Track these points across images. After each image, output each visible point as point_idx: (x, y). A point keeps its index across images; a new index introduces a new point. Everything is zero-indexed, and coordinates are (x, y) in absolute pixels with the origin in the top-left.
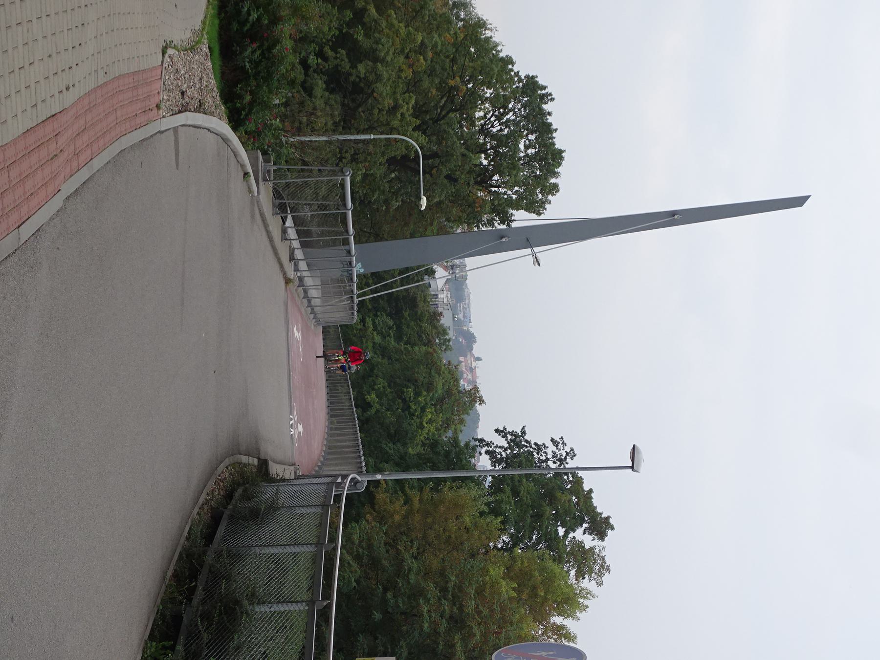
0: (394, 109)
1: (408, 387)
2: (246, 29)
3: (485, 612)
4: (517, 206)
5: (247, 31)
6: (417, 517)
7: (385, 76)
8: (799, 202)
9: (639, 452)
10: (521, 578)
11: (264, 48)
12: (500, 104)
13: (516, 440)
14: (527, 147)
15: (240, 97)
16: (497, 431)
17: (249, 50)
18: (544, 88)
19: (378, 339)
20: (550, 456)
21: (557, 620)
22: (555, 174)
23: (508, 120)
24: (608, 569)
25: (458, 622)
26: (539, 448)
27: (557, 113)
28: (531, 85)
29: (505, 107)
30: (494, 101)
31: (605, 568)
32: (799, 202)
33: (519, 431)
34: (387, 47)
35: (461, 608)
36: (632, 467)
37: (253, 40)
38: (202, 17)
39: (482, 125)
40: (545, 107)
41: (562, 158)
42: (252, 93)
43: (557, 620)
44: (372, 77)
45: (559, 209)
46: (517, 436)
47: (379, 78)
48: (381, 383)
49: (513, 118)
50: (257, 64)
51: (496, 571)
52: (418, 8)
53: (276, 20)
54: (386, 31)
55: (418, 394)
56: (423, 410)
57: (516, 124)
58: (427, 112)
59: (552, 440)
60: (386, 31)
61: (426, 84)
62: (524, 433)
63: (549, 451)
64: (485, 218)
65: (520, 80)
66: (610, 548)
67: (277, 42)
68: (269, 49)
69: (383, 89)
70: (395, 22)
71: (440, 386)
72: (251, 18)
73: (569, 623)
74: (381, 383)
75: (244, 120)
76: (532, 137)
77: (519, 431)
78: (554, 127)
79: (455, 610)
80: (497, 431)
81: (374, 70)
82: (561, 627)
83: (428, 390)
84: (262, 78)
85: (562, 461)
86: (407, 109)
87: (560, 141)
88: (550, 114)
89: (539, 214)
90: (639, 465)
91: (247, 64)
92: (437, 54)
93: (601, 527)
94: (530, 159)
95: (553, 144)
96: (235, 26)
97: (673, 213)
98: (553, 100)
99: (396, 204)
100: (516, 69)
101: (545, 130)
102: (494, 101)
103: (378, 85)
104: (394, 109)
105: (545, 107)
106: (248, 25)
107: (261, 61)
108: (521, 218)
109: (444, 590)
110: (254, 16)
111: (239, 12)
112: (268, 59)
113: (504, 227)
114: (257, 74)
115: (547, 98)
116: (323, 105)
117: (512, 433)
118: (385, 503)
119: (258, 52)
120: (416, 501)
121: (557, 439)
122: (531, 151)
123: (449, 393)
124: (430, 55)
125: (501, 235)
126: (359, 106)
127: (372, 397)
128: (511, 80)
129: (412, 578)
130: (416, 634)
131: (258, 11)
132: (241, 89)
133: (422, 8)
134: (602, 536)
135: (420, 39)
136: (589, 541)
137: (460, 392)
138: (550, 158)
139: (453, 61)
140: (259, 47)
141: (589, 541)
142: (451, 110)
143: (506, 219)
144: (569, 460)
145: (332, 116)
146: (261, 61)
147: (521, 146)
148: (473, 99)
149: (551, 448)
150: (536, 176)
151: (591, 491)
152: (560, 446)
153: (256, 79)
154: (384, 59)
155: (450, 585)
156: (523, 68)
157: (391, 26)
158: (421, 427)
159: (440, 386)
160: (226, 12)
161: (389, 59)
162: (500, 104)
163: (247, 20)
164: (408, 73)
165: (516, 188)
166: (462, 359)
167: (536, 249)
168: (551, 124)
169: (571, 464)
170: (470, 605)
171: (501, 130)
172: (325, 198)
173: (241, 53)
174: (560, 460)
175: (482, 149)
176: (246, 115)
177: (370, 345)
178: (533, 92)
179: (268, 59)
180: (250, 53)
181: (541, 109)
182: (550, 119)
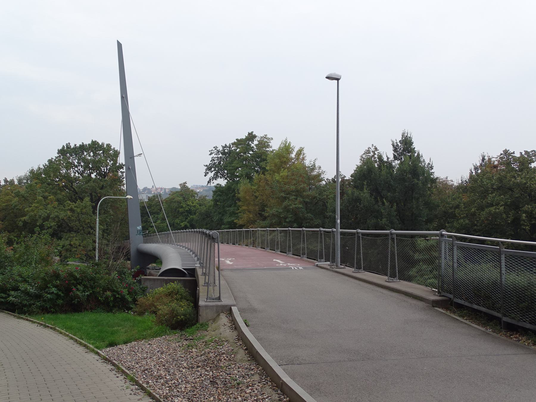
0: (72, 210)
1: (179, 211)
2: (62, 295)
3: (295, 182)
4: (116, 162)
5: (63, 293)
6: (250, 207)
7: (56, 214)
8: (120, 45)
9: (331, 74)
10: (278, 168)
11: (75, 282)
12: (70, 165)
13: (209, 168)
14: (90, 156)
15: (107, 298)
16: (205, 176)
17: (78, 293)
18: (64, 146)
19: (159, 221)
20: (216, 156)
21: (293, 155)
22: (103, 144)
23: (78, 163)
24: (266, 135)
25: (298, 193)
26: (213, 160)
27: (75, 142)
28: (62, 152)
29: (71, 163)
30: (67, 168)
31: (265, 137)
32: (120, 45)
33: (206, 167)
34: (43, 213)
35: (293, 191)
36: (338, 79)
37: (71, 290)
38: (81, 349)
39: (79, 173)
40: (72, 147)
41: (95, 141)
42: (105, 290)
43: (293, 155)
44: (57, 219)
45: (118, 144)
46: (208, 168)
47: (57, 217)
48: (177, 221)
49: (77, 161)
50: (85, 286)
51: (277, 177)
52: (23, 199)
53: (56, 275)
54: (35, 212)
55: (182, 207)
56: (188, 205)
57: (79, 160)
58: (71, 197)
59: (210, 155)
60: (35, 212)
61: (60, 196)
62: (206, 166)
63: (215, 156)
64: (120, 174)
65: (60, 156)
66: (259, 134)
67: (71, 275)
68: (76, 279)
69: (62, 215)
70: (31, 209)
71: (180, 198)
72: (55, 292)
73: (296, 150)
74: (177, 221)
75: (121, 295)
76: (85, 153)
77: (206, 167)
78: (81, 144)
79: (294, 194)
80: (205, 176)
81: (54, 219)
82: (298, 152)
83: (181, 203)
84: (94, 283)
85: (218, 151)
86: (73, 205)
87: (87, 142)
88: (75, 145)
89: (119, 153)
90: (338, 75)
91: (87, 293)
92: (46, 191)
93: (251, 137)
94: (95, 154)
95: (89, 144)
96: (60, 302)
97: (122, 97)
98: (69, 143)
99: (111, 212)
100: (55, 158)
101: (83, 148)
102: (67, 168)
103: (60, 217)
104: (72, 210)
105: (72, 147)
106: (60, 293)
107: (84, 285)
108: (121, 159)
109: (285, 198)
110: (54, 290)
111: (51, 300)
112: (82, 280)
113: (124, 167)
114: (92, 288)
115: (68, 146)
116: (68, 241)
117: (206, 170)
118: (244, 220)
119: (79, 287)
120: (244, 208)
121: (209, 153)
122: (92, 154)
123: (182, 195)
124: (47, 194)
125: (128, 169)
126: (68, 225)
127: (183, 225)
128: (60, 160)
129: (280, 211)
130: (303, 210)
131: (49, 288)
132: (101, 297)
133: (23, 197)
134: (255, 137)
135: (40, 198)
136: (256, 142)
137: (181, 191)
138: (95, 146)
139: (49, 184)
140: (75, 287)
141: (256, 142)
142: (72, 187)
143: (121, 166)
144: (218, 149)
145: (73, 237)
146: (84, 285)
147: (89, 158)
148: (67, 177)
149: (213, 155)
150: (103, 153)
151: (237, 140)
152: (213, 152)
153: (95, 287)
154: (48, 214)
155: (284, 195)
156: (54, 155)
157: (33, 211)
158: (195, 206)
159: (180, 198)
160: (50, 307)
161: (48, 212)
162: (70, 165)
163: (57, 294)
164: (56, 203)
165: (108, 161)
166: (153, 192)
167: (135, 154)
168: (80, 145)
169: (220, 148)
170: (293, 187)
171: (82, 166)
172: (109, 241)
173: (79, 298)
174: (218, 152)
175: (90, 175)
176: (119, 294)
177: (162, 224)
178: (65, 152)
179: (82, 280)
180: (80, 293)
181: (73, 148)
182: (78, 145)
